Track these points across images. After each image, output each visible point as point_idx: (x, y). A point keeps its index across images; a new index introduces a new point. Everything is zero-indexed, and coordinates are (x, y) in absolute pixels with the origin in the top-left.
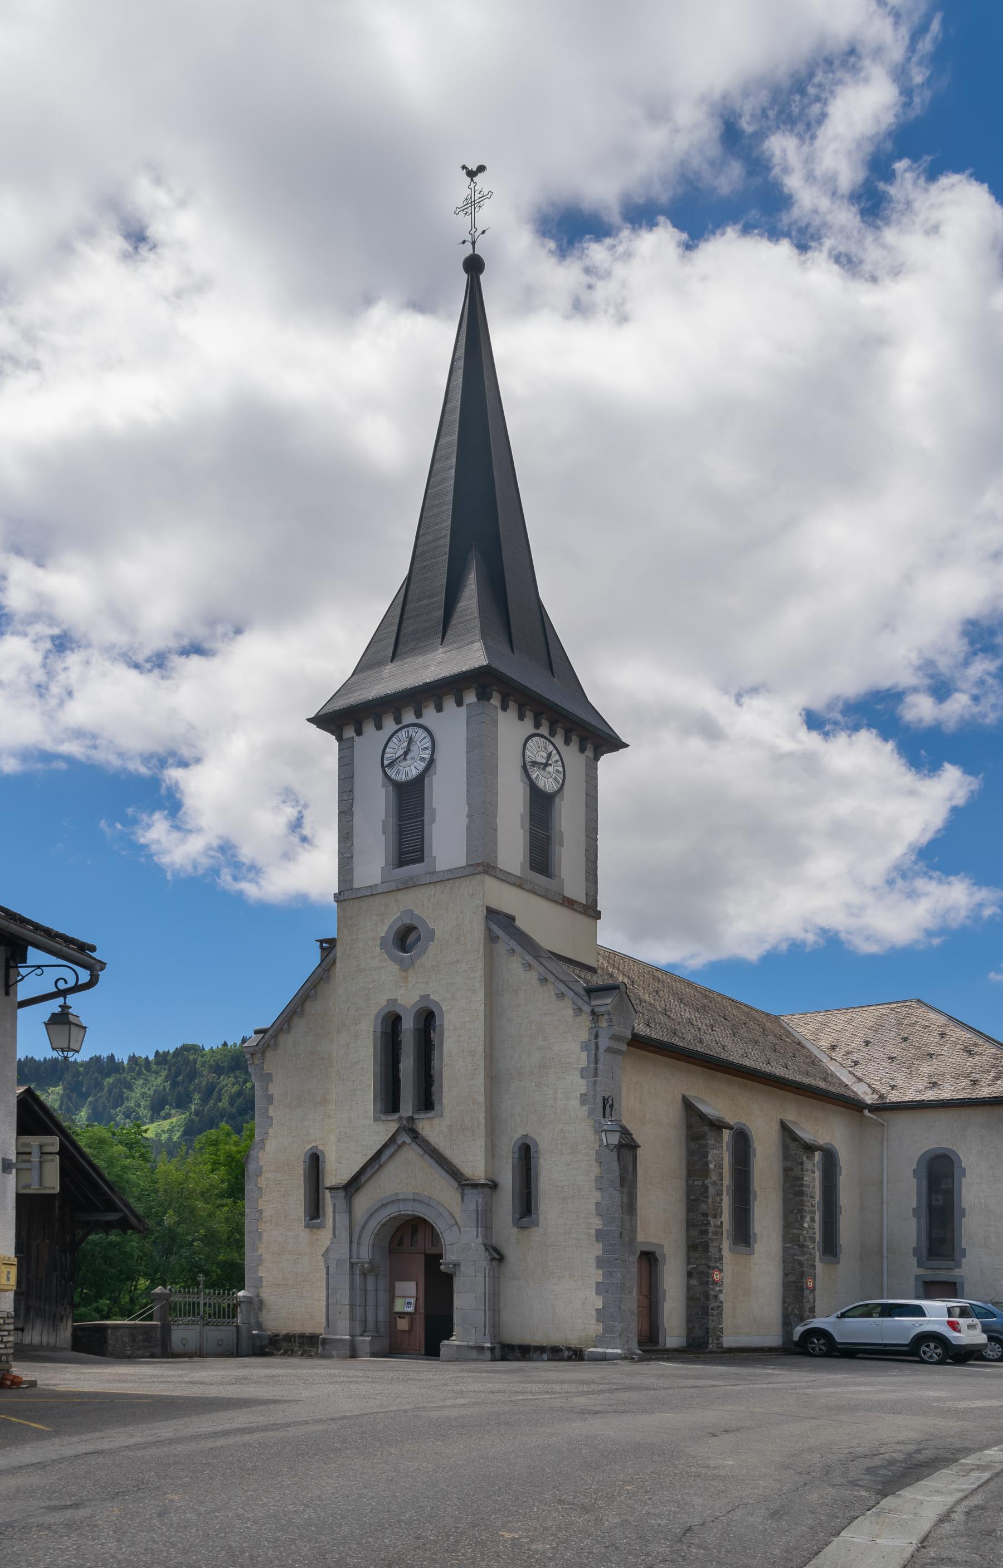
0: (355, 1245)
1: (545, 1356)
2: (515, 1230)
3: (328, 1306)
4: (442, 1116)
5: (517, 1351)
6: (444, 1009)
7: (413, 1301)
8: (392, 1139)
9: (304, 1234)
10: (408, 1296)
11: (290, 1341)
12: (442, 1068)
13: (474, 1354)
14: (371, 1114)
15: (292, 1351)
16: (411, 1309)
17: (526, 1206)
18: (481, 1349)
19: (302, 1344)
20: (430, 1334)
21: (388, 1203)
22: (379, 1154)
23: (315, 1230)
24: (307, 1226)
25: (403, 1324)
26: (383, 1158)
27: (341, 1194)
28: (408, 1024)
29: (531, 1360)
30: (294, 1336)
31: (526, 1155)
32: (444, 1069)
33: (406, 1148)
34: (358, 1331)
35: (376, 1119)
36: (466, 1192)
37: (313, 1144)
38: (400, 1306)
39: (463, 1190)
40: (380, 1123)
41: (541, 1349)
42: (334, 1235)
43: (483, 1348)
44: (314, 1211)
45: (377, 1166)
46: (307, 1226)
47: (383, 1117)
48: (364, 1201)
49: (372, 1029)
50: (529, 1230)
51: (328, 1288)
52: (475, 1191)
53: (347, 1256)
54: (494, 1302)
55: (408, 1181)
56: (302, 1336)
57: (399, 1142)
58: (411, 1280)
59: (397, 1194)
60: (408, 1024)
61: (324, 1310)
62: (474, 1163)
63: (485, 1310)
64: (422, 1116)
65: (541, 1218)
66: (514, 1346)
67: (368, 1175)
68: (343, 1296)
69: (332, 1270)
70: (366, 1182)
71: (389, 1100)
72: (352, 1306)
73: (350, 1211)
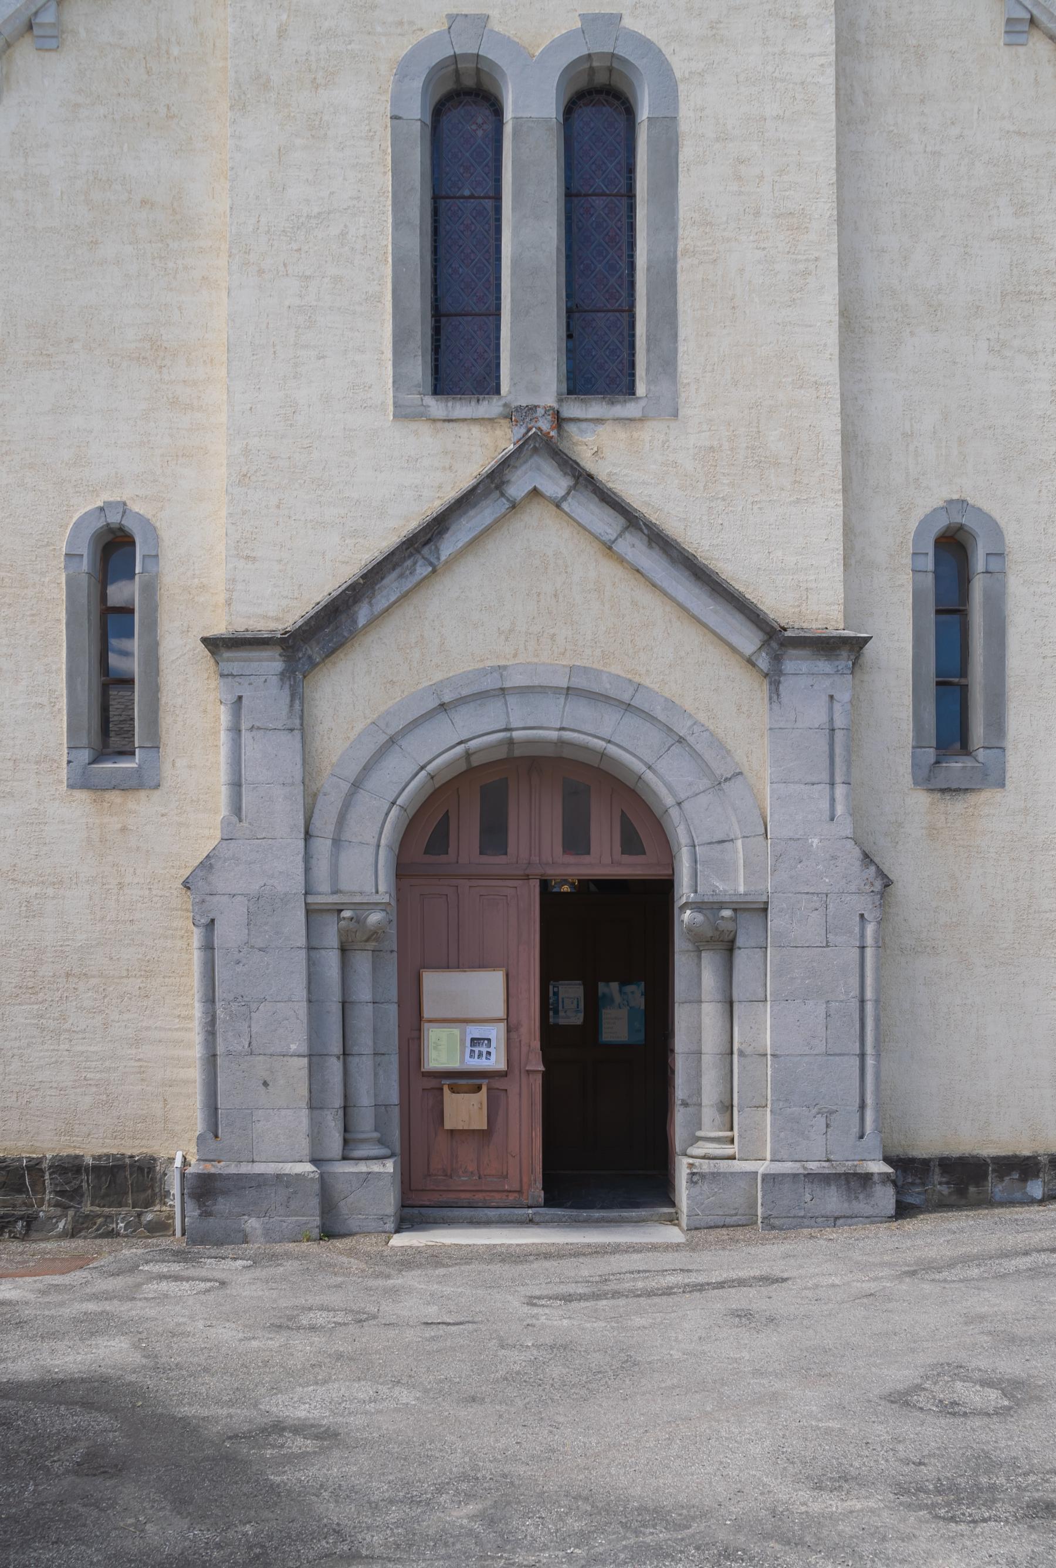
0: (322, 846)
1: (1036, 1189)
2: (921, 799)
3: (211, 1060)
4: (675, 415)
5: (937, 1177)
6: (679, 68)
7: (496, 1033)
8: (494, 481)
9: (72, 813)
10: (479, 1019)
11: (20, 1189)
12: (674, 261)
13: (833, 1200)
14: (384, 391)
15: (30, 1221)
16: (496, 1061)
17: (956, 720)
18: (858, 1182)
19: (69, 1196)
20: (604, 1134)
21: (462, 701)
22: (436, 527)
23: (115, 797)
24: (81, 782)
25: (465, 1111)
26: (448, 546)
27: (271, 664)
28: (531, 105)
29: (988, 1203)
30: (35, 1167)
31: (954, 554)
32: (682, 263)
33: (537, 515)
34: (334, 1143)
35: (403, 413)
36: (789, 666)
37: (106, 497)
38: (443, 1051)
39: (777, 659)
40: (424, 428)
41: (1021, 1167)
42: (237, 809)
43: (866, 1179)
44: (112, 722)
45: (422, 570)
46: (81, 782)
47: (436, 407)
48: (355, 695)
49: (384, 108)
50: (972, 798)
51: (210, 1000)
52: (823, 665)
53: (298, 884)
54: (875, 1026)
55: (536, 627)
56: (69, 1169)
57: (518, 486)
58: (483, 965)
59: (502, 668)
60: (531, 105)
61: (195, 1074)
62: (802, 580)
63: (862, 1056)
64: (596, 409)
65: (1014, 762)
66: (926, 1163)
67: (381, 602)
68: (284, 1025)
69: (229, 933)
70: (375, 620)
71: (453, 351)
72: (315, 1057)
73: (301, 725)
